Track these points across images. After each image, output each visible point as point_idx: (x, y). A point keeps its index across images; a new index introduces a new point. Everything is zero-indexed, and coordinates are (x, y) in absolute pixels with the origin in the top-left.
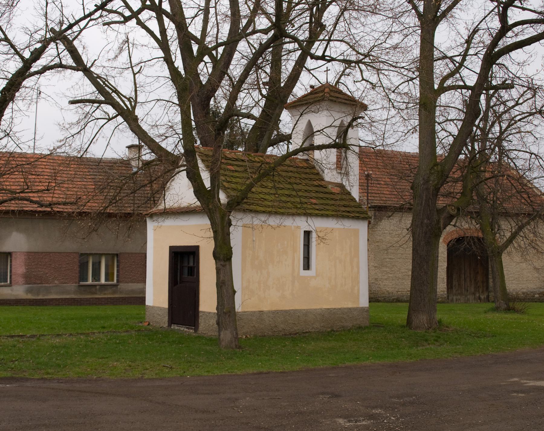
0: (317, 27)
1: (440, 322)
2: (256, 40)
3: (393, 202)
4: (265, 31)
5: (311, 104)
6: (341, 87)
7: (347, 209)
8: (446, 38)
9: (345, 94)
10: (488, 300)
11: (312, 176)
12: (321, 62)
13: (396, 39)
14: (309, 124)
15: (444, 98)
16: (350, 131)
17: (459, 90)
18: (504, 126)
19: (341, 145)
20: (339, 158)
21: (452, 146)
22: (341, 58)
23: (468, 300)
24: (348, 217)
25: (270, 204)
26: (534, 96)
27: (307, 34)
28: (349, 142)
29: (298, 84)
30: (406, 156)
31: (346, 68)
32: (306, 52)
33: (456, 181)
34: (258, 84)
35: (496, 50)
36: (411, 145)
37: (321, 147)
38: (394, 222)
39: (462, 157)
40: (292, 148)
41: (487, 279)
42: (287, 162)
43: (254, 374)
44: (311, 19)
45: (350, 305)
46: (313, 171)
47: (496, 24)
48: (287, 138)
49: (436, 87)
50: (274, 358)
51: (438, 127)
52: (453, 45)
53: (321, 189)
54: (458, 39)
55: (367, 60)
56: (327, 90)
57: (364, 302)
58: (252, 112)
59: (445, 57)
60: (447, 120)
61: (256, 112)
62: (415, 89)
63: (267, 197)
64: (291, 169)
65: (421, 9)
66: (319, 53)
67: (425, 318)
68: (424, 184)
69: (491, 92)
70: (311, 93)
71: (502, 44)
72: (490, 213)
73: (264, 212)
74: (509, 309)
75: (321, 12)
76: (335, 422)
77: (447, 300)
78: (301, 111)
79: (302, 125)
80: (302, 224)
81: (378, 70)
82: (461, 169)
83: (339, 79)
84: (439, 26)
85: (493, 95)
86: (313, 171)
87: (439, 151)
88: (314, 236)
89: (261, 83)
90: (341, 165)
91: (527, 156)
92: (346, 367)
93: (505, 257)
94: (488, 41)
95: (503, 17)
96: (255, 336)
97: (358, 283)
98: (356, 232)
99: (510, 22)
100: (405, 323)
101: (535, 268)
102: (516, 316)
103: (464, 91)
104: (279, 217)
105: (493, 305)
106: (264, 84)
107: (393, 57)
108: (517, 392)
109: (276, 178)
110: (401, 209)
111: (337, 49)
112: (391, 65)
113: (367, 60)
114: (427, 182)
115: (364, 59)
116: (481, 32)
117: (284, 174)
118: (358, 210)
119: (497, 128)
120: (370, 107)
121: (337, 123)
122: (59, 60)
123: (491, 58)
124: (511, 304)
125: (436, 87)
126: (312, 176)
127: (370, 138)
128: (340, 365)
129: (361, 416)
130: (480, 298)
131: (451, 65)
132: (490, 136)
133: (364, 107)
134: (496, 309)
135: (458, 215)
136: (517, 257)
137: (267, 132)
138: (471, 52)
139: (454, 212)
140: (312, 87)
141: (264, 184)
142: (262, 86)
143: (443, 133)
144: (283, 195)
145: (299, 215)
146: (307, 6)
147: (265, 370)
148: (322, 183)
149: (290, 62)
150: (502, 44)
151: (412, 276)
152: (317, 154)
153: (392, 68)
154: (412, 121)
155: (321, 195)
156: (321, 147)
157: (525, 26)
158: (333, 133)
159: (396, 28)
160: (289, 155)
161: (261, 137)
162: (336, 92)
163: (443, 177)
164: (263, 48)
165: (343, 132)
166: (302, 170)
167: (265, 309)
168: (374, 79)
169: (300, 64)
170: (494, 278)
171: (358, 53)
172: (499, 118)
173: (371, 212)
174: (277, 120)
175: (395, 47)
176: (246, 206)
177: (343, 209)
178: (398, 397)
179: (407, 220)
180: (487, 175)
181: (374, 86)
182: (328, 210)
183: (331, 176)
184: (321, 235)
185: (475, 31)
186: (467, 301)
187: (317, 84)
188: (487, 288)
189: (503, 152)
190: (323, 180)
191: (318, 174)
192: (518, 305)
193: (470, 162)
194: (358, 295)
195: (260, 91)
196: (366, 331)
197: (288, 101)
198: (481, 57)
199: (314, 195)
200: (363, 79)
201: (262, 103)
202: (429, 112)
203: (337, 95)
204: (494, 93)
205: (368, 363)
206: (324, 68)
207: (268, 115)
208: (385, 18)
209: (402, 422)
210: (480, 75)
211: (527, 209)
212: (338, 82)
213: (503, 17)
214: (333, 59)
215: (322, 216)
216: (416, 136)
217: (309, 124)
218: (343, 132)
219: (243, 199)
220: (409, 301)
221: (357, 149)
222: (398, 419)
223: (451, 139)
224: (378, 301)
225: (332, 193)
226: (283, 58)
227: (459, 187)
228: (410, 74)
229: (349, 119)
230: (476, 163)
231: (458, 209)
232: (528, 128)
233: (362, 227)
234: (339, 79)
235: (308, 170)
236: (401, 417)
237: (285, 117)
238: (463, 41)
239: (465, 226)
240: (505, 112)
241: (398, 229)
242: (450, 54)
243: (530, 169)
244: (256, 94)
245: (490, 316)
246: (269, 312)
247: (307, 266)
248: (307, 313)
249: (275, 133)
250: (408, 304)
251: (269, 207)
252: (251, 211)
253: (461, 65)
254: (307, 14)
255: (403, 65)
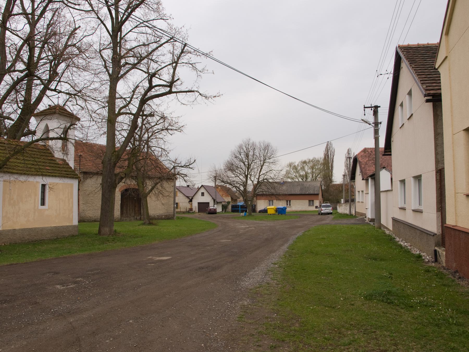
0: (54, 74)
1: (115, 231)
2: (16, 75)
3: (93, 170)
4: (21, 71)
5: (47, 115)
6: (66, 107)
7: (67, 173)
8: (123, 88)
9: (68, 111)
10: (140, 219)
11: (47, 154)
12: (54, 93)
13: (97, 85)
14: (47, 126)
15: (120, 118)
16: (69, 130)
17: (128, 115)
18: (150, 134)
19: (64, 138)
20: (63, 144)
21: (124, 142)
22: (68, 92)
23: (131, 220)
24: (67, 177)
25: (20, 169)
26: (164, 121)
27: (48, 76)
28: (67, 137)
29: (41, 103)
30: (101, 146)
31: (70, 98)
32: (46, 88)
33: (125, 160)
34: (17, 101)
35: (146, 97)
36: (103, 141)
37: (52, 139)
38: (94, 180)
39: (128, 148)
40: (35, 138)
41: (141, 209)
42: (32, 146)
43: (7, 265)
44: (50, 68)
45: (68, 224)
46: (48, 151)
47: (147, 85)
48: (34, 133)
49: (116, 112)
50: (21, 255)
51: (117, 133)
52: (126, 92)
53: (52, 162)
54: (128, 89)
55: (79, 94)
56: (58, 108)
57: (75, 222)
58: (10, 116)
59: (121, 98)
60: (123, 130)
61: (15, 117)
62: (105, 112)
63: (19, 165)
64: (35, 150)
65: (111, 72)
66: (53, 87)
67: (108, 229)
68: (108, 161)
69: (144, 117)
70: (48, 109)
71: (149, 94)
72: (141, 177)
73: (17, 173)
74: (150, 224)
75: (57, 65)
76: (55, 287)
77: (120, 220)
78: (41, 118)
79: (42, 126)
80: (40, 180)
81: (86, 100)
82: (128, 154)
83: (66, 103)
84: (119, 82)
85: (145, 119)
86: (48, 151)
87: (118, 145)
88: (47, 187)
89: (18, 100)
90: (64, 149)
91: (160, 150)
92: (64, 257)
93: (148, 198)
94: (143, 92)
95: (150, 82)
96: (10, 243)
97: (72, 212)
98: (72, 185)
99: (154, 84)
100: (97, 232)
101: (163, 204)
102: (153, 227)
103: (130, 115)
104: (26, 176)
105: (142, 222)
106: (21, 101)
107: (95, 95)
108: (151, 263)
109: (25, 154)
110: (97, 174)
111: (64, 87)
112: (93, 98)
113: (79, 94)
114: (110, 160)
115: (77, 94)
116: (140, 87)
117: (30, 152)
118: (73, 173)
119: (146, 136)
120: (81, 120)
121: (63, 126)
122: (21, 69)
123: (143, 101)
124: (151, 221)
125: (116, 112)
126: (47, 154)
127: (81, 136)
128: (60, 256)
129: (70, 283)
130: (137, 219)
131: (124, 102)
132: (143, 139)
133: (79, 119)
134: (144, 224)
135: (125, 177)
136: (154, 198)
137: (21, 129)
138: (135, 97)
139: (123, 176)
140: (49, 106)
141: (18, 157)
142: (19, 102)
143: (120, 135)
144: (29, 164)
145: (39, 175)
146: (48, 61)
147: (15, 263)
148: (53, 158)
149: (37, 90)
150: (149, 94)
151: (101, 208)
152: (50, 143)
153: (92, 100)
154: (103, 129)
155: (52, 165)
156: (52, 139)
157: (160, 87)
158: (60, 131)
159: (96, 79)
160: (33, 142)
161: (18, 131)
162: (62, 109)
163: (118, 158)
164: (20, 80)
165: (66, 131)
166: (41, 151)
167: (17, 228)
168: (83, 105)
169: (43, 93)
170: (143, 209)
171: (76, 90)
172: (147, 130)
173: (81, 175)
174: (28, 123)
175: (95, 89)
176: (5, 170)
177: (65, 173)
178: (91, 271)
179: (100, 180)
180: (141, 158)
181: (83, 108)
182: (56, 173)
183: (58, 155)
184: (51, 186)
185: (137, 87)
186: (130, 220)
187: (53, 105)
188: (140, 213)
189: (149, 147)
190: (54, 157)
191: (51, 153)
192: (154, 222)
193: (132, 151)
194: (72, 219)
195: (18, 105)
196: (76, 237)
197: (35, 112)
198: (139, 99)
199: (48, 165)
200: (77, 104)
201: (19, 111)
202: (112, 125)
203: (64, 111)
204: (146, 118)
205: (76, 254)
206: (57, 96)
207: (22, 119)
208: (90, 74)
209: (92, 284)
210: (138, 108)
211: (158, 175)
212: (64, 105)
213: (150, 82)
214: (60, 92)
215: (52, 176)
216: (106, 135)
217: (47, 126)
218: (66, 131)
219: (4, 165)
220: (100, 221)
221: (73, 141)
222: (90, 282)
223: (124, 139)
224: (84, 221)
225: (58, 164)
226: (33, 88)
227: (126, 163)
228: (103, 105)
229: (68, 125)
230: (135, 152)
231: (126, 174)
232: (161, 136)
233: (75, 183)
234: (66, 103)
235: (45, 151)
236: (92, 281)
237: (33, 121)
238: (131, 91)
239: (132, 183)
240: (150, 128)
241: (94, 184)
242: (124, 97)
243: (161, 156)
244: (15, 106)
245: (141, 227)
246: (19, 229)
247: (43, 203)
248: (42, 229)
249: (26, 129)
250: (99, 223)
251: (20, 170)
252: (9, 172)
253: (130, 102)
254: (48, 65)
255: (99, 99)
